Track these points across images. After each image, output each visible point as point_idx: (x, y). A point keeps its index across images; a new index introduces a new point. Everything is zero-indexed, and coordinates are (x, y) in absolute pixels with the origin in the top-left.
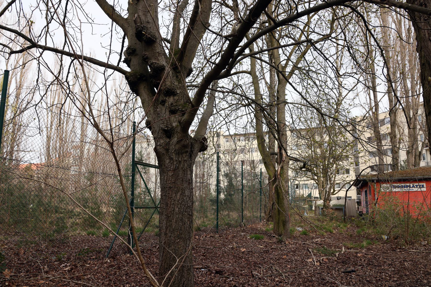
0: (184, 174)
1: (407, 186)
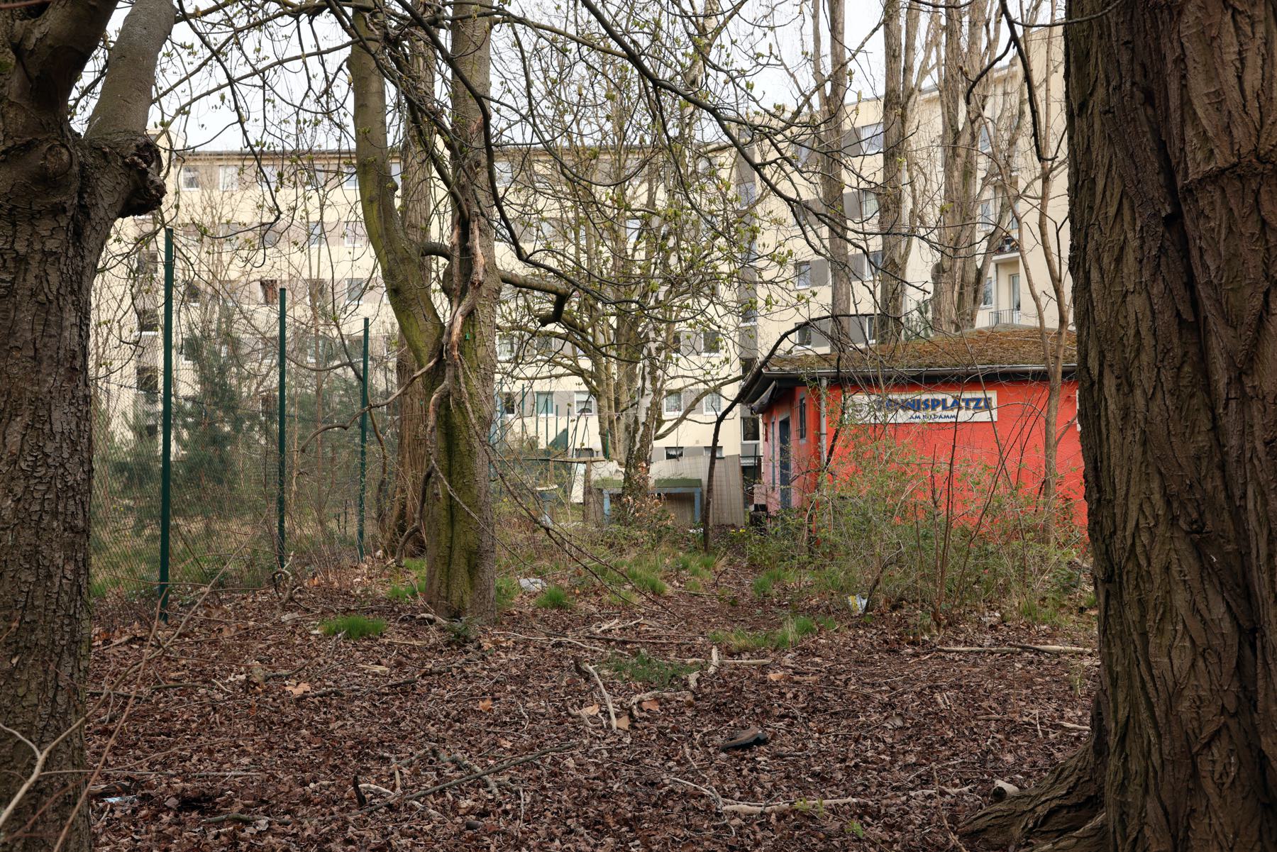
0: (46, 324)
1: (935, 404)
